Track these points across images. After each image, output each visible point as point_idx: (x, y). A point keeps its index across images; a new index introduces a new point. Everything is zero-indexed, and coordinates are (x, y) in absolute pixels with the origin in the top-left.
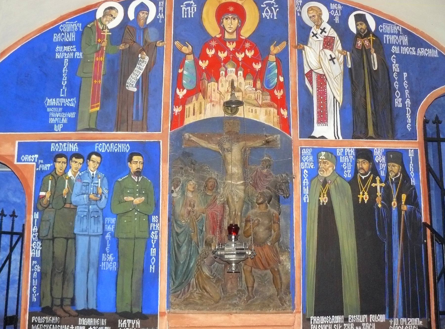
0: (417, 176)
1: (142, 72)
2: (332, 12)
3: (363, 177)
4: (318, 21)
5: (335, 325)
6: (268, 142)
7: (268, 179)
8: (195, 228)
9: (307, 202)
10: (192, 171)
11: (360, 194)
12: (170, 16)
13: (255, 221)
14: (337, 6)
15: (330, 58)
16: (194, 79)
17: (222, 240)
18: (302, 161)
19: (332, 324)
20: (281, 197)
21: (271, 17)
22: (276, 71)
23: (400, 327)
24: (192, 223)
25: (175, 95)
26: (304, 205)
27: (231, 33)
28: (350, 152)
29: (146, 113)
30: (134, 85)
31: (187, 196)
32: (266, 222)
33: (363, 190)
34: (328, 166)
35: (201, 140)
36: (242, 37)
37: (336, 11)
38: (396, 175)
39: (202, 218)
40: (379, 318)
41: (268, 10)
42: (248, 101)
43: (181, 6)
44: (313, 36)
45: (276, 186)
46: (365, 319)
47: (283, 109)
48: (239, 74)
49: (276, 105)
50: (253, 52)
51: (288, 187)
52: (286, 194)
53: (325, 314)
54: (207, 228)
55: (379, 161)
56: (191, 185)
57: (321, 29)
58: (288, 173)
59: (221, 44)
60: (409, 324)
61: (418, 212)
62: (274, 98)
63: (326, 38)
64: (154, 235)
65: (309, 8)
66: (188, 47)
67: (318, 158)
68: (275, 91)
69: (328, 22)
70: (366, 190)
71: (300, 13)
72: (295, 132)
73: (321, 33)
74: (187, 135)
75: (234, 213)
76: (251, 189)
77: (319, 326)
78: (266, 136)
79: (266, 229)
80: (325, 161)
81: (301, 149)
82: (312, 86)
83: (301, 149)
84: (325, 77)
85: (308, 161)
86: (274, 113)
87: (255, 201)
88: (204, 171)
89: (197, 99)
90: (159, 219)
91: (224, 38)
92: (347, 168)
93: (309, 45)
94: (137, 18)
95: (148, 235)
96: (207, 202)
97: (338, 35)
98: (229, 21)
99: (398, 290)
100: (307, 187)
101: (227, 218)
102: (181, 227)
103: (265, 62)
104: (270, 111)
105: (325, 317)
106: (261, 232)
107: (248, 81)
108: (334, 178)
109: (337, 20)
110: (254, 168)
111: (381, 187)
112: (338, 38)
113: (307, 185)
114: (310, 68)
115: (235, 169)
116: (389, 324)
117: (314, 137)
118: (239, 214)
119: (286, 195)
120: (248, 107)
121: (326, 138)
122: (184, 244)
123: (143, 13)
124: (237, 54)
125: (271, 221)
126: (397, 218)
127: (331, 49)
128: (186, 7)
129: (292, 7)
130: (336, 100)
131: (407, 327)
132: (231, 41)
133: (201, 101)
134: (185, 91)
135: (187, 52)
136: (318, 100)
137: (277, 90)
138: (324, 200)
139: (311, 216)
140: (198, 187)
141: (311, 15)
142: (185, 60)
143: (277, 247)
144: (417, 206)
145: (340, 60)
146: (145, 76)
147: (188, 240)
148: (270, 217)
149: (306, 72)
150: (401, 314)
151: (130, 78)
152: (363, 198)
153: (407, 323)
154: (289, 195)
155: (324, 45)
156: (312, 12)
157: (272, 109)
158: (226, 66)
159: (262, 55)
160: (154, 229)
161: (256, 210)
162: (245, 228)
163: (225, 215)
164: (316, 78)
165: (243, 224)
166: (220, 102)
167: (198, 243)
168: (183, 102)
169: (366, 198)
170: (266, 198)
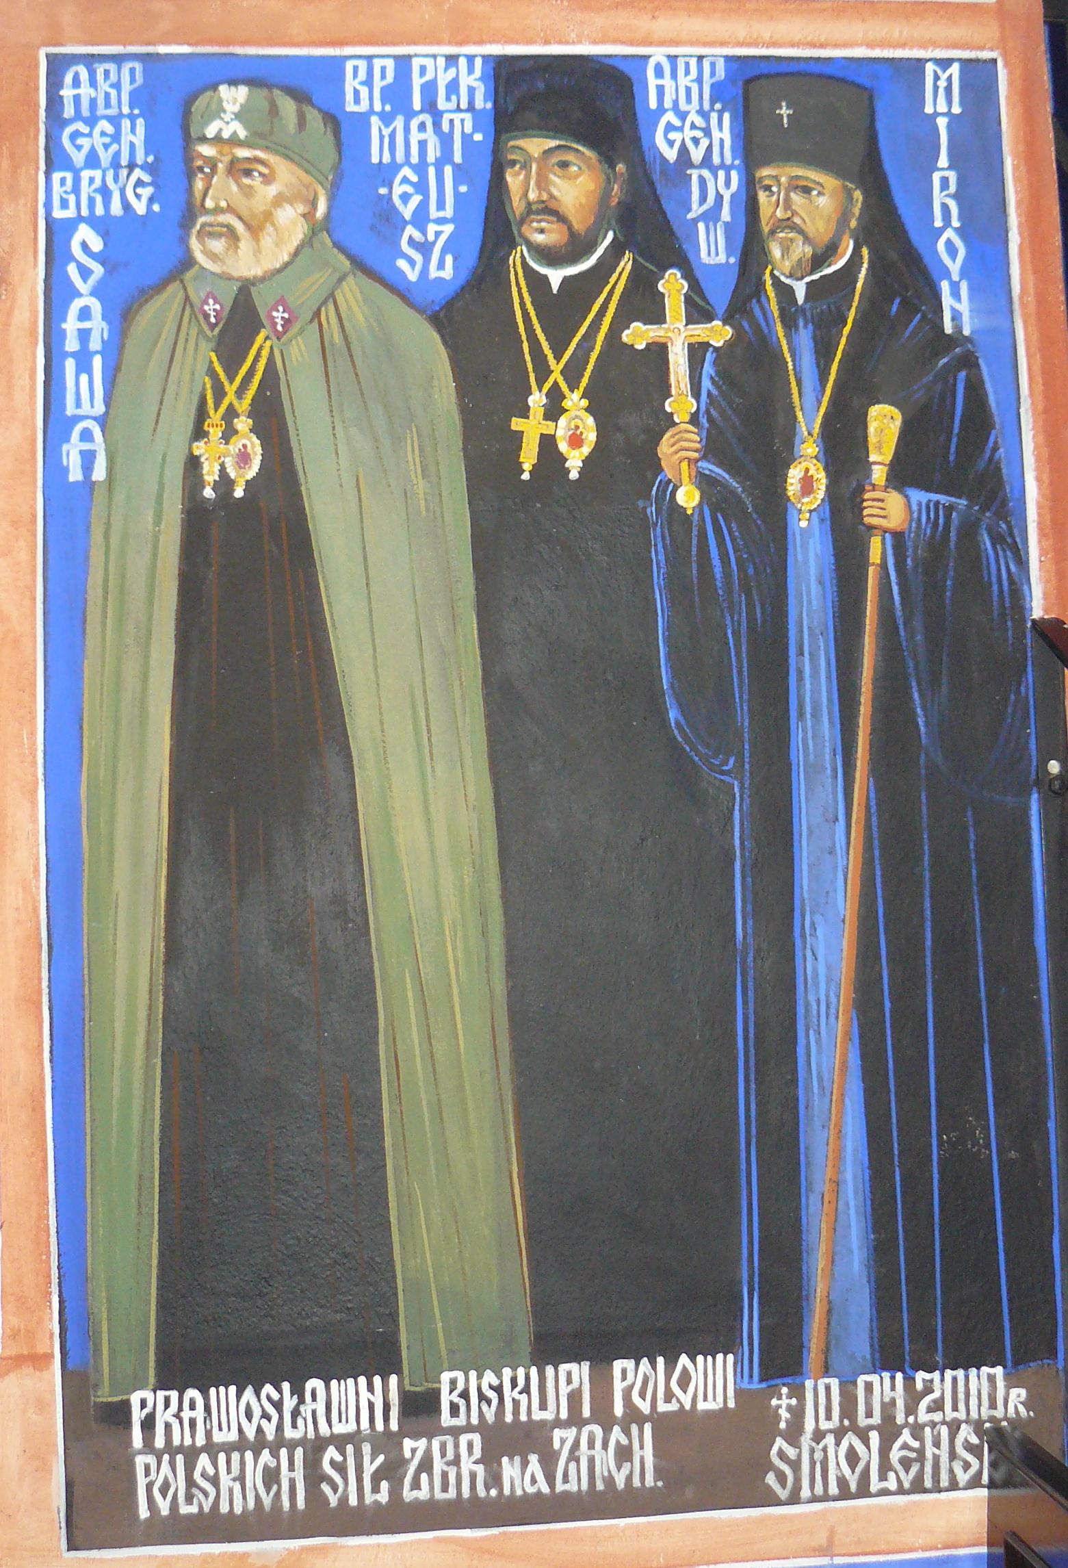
0: (987, 267)
3: (556, 277)
5: (331, 1453)
9: (88, 484)
11: (524, 412)
18: (55, 159)
19: (303, 1442)
23: (851, 1439)
28: (453, 87)
33: (556, 376)
34: (272, 190)
38: (819, 261)
40: (684, 1381)
46: (575, 1399)
53: (246, 1364)
55: (684, 151)
60: (923, 1417)
61: (997, 539)
67: (188, 139)
70: (572, 374)
77: (204, 1461)
80: (243, 153)
81: (57, 66)
83: (57, 66)
85: (105, 157)
92: (423, 207)
99: (839, 1158)
100: (97, 362)
105: (249, 1393)
108: (319, 281)
111: (697, 352)
113: (95, 344)
116: (766, 1426)
126: (831, 590)
131: (906, 1436)
138: (233, 458)
139: (122, 590)
144: (991, 492)
150: (860, 1340)
152: (548, 442)
153: (911, 1410)
169: (576, 441)
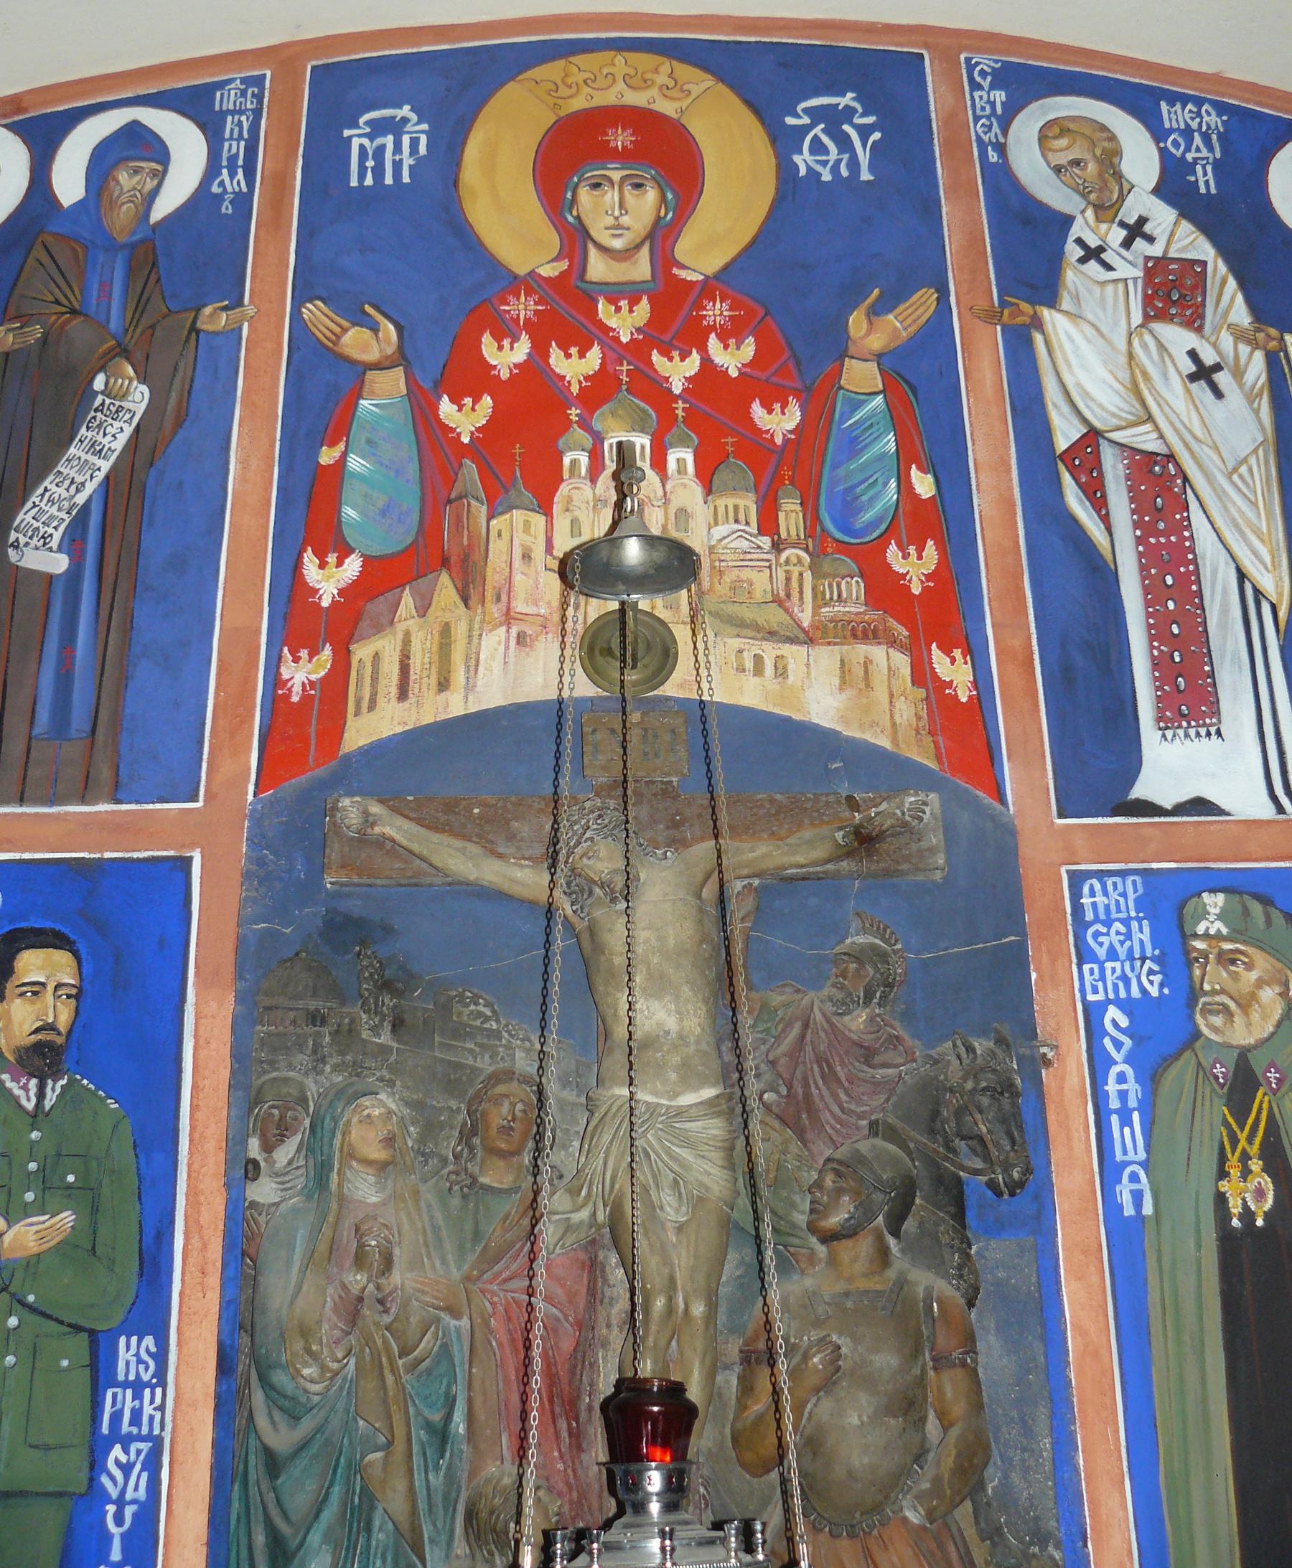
1: (106, 466)
2: (1175, 143)
4: (1104, 187)
6: (864, 841)
7: (879, 1073)
8: (397, 1419)
10: (385, 1038)
12: (280, 183)
13: (806, 1357)
14: (1199, 114)
15: (1193, 368)
16: (411, 501)
17: (583, 1495)
18: (1084, 954)
20: (975, 1187)
21: (844, 172)
22: (889, 443)
24: (370, 1384)
25: (292, 591)
26: (1126, 1237)
27: (627, 254)
29: (119, 697)
30: (57, 536)
31: (342, 1199)
32: (886, 1361)
34: (1254, 975)
35: (436, 838)
36: (683, 274)
37: (1198, 140)
39: (445, 1347)
41: (825, 139)
42: (731, 609)
43: (347, 133)
44: (1083, 260)
45: (935, 1114)
47: (947, 651)
48: (672, 465)
49: (902, 632)
50: (749, 349)
51: (1012, 1123)
52: (1007, 1169)
54: (481, 1415)
56: (375, 1117)
57: (1122, 224)
58: (1006, 1030)
59: (567, 310)
62: (885, 590)
63: (1155, 268)
64: (126, 1469)
65: (1049, 124)
66: (375, 329)
67: (1185, 936)
68: (892, 552)
69: (1157, 191)
71: (1001, 149)
72: (1027, 779)
73: (1127, 243)
74: (350, 809)
75: (659, 1303)
76: (768, 1141)
78: (852, 803)
79: (889, 1411)
80: (1227, 946)
82: (1106, 520)
83: (1077, 880)
84: (1177, 465)
86: (892, 672)
87: (801, 1219)
88: (460, 1032)
89: (423, 610)
90: (161, 1357)
91: (582, 276)
93: (1066, 303)
94: (99, 195)
95: (84, 1476)
96: (477, 1235)
97: (1224, 251)
98: (611, 196)
100: (1136, 1116)
101: (617, 1338)
102: (292, 1409)
103: (820, 399)
104: (867, 663)
106: (856, 1431)
107: (725, 502)
109: (1205, 180)
110: (786, 1005)
112: (1222, 268)
113: (1132, 1103)
114: (1085, 420)
115: (666, 1012)
117: (1146, 808)
118: (698, 1309)
119: (1007, 1169)
120: (736, 643)
121: (1228, 814)
122: (315, 1538)
123: (136, 171)
124: (655, 356)
125: (916, 1352)
127: (1194, 322)
128: (371, 137)
129: (954, 122)
130: (1258, 593)
132: (622, 294)
133: (447, 617)
134: (353, 566)
135: (373, 355)
136: (1146, 591)
137: (901, 547)
140: (422, 1140)
141: (1062, 159)
142: (360, 396)
143: (970, 1533)
145: (1249, 377)
146: (126, 488)
147: (345, 1502)
148: (906, 1320)
149: (1062, 444)
151: (34, 498)
154: (1027, 1171)
155: (1148, 301)
156: (1063, 142)
157: (878, 653)
158: (597, 424)
159: (799, 359)
160: (125, 1427)
161: (808, 1282)
162: (742, 1407)
163: (601, 1321)
164: (1121, 470)
165: (730, 1381)
166: (563, 620)
167: (416, 1530)
168: (345, 624)
170: (878, 1197)
